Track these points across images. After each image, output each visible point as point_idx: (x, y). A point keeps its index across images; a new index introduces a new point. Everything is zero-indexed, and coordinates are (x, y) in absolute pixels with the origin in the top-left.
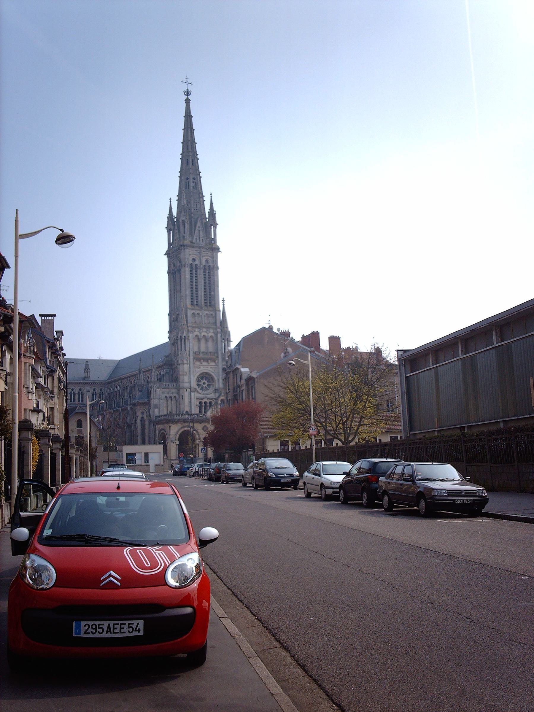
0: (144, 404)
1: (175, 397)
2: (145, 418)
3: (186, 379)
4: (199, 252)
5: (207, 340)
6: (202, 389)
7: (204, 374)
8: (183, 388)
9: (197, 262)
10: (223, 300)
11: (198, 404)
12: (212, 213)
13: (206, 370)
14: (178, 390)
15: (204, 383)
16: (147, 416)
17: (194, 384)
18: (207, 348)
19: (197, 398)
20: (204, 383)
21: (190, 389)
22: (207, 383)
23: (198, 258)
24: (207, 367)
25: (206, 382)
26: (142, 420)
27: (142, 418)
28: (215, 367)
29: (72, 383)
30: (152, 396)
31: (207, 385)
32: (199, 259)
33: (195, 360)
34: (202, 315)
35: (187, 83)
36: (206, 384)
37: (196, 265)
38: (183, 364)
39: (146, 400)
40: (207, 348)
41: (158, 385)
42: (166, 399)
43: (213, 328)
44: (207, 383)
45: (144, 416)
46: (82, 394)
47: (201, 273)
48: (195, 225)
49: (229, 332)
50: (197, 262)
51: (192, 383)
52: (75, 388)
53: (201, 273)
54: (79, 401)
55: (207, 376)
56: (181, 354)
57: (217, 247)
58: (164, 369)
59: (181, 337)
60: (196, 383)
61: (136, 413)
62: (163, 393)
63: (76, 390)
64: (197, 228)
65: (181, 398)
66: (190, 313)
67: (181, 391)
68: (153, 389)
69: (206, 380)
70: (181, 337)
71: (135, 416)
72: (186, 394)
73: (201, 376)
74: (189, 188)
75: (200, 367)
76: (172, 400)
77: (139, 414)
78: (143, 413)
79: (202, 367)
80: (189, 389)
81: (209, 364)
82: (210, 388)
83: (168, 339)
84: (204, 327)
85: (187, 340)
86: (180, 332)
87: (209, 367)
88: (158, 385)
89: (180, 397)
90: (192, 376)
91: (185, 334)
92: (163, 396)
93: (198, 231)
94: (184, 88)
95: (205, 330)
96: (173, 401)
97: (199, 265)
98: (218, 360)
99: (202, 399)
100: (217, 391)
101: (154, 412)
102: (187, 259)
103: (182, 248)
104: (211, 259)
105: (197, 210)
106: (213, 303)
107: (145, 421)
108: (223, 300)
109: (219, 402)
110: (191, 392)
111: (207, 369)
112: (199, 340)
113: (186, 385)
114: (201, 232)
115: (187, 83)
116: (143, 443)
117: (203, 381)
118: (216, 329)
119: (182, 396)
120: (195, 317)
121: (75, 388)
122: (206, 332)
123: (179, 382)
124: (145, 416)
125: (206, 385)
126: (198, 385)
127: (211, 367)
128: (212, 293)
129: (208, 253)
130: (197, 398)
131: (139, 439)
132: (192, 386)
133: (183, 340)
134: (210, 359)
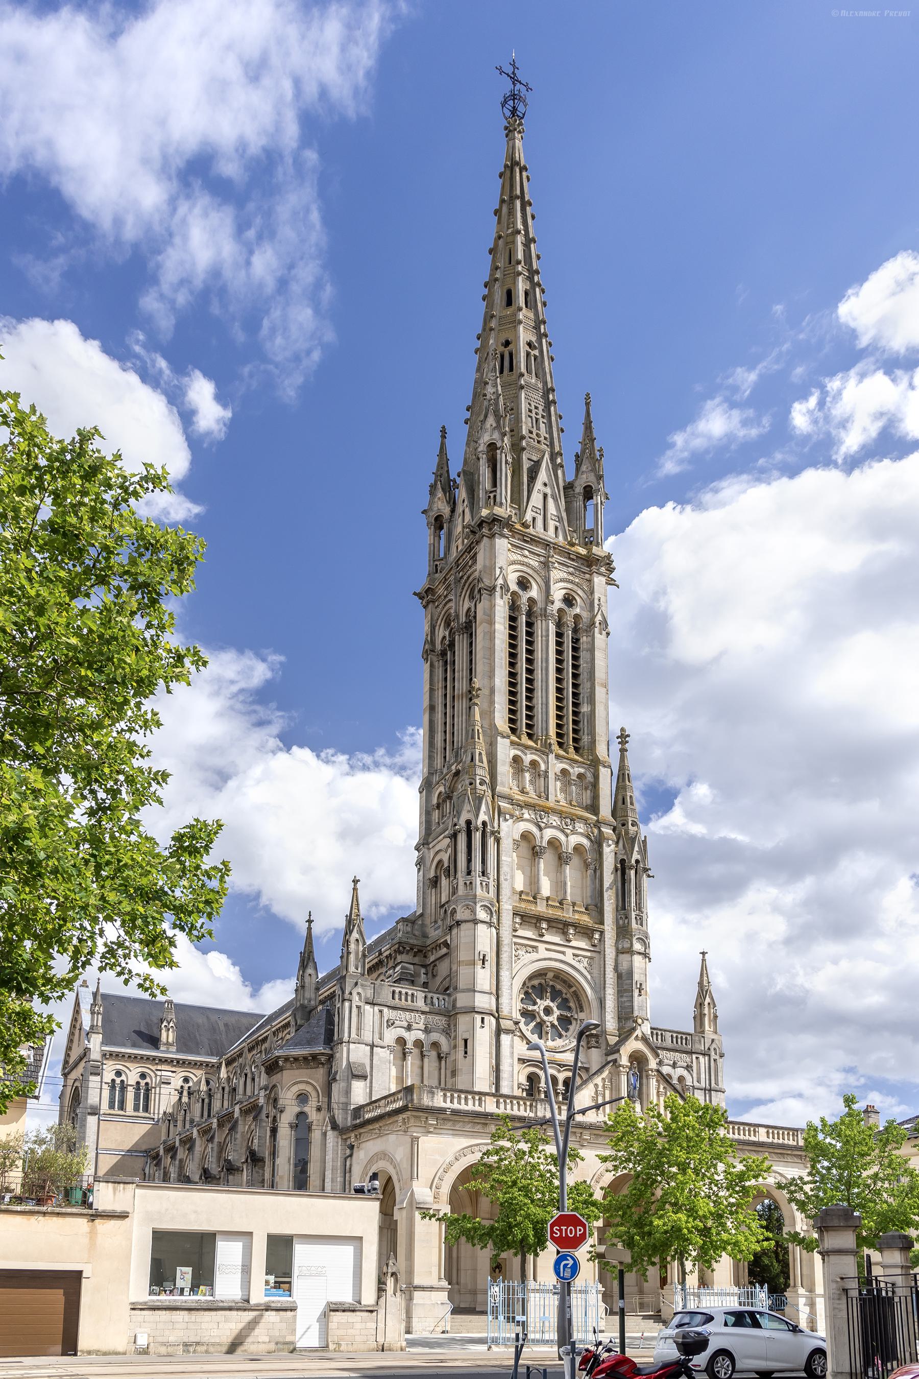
0: (312, 1060)
1: (435, 1045)
2: (313, 1116)
3: (484, 978)
4: (542, 559)
5: (562, 859)
6: (540, 1029)
7: (550, 975)
8: (472, 1010)
9: (534, 592)
11: (523, 1080)
13: (556, 960)
14: (451, 1014)
15: (548, 1011)
16: (319, 1109)
17: (512, 1004)
19: (519, 1059)
20: (548, 1011)
21: (497, 1019)
22: (557, 1013)
23: (539, 579)
24: (563, 953)
25: (553, 1005)
26: (301, 1124)
27: (301, 1115)
28: (590, 958)
29: (123, 1056)
30: (348, 1027)
31: (558, 1019)
32: (543, 584)
33: (518, 920)
34: (546, 772)
35: (514, 80)
36: (555, 1016)
37: (531, 601)
38: (475, 922)
39: (320, 1049)
41: (369, 993)
42: (398, 1048)
43: (585, 821)
44: (557, 1013)
45: (306, 1109)
46: (148, 1090)
47: (547, 632)
48: (532, 478)
50: (534, 592)
51: (504, 1000)
52: (127, 1071)
53: (547, 632)
54: (136, 1108)
55: (558, 987)
56: (470, 885)
58: (394, 968)
59: (468, 823)
60: (520, 1006)
61: (275, 1100)
62: (391, 1024)
63: (132, 1076)
64: (538, 485)
65: (461, 1048)
66: (505, 751)
67: (462, 1020)
68: (347, 1004)
69: (552, 1001)
70: (468, 823)
71: (273, 1112)
72: (483, 1037)
73: (536, 982)
76: (422, 1056)
77: (288, 1097)
78: (302, 1098)
79: (542, 947)
80: (493, 1021)
81: (569, 941)
82: (567, 1030)
84: (554, 811)
85: (491, 841)
86: (466, 807)
87: (569, 952)
88: (369, 993)
89: (455, 1047)
90: (505, 974)
91: (483, 817)
92: (390, 1036)
93: (541, 497)
94: (507, 86)
95: (555, 820)
96: (426, 1060)
97: (540, 605)
99: (540, 1064)
100: (593, 1042)
101: (348, 1092)
102: (501, 568)
103: (485, 531)
105: (538, 435)
106: (585, 739)
107: (309, 1128)
109: (624, 1061)
110: (499, 1031)
111: (560, 957)
112: (535, 853)
113: (483, 1001)
114: (551, 503)
115: (514, 80)
116: (301, 1183)
117: (542, 1004)
118: (598, 824)
119: (466, 1041)
120: (522, 770)
121: (127, 1071)
123: (456, 988)
124: (310, 1109)
125: (553, 1018)
126: (525, 1013)
127: (574, 955)
130: (522, 1061)
131: (284, 1164)
132: (505, 1011)
133: (477, 836)
134: (575, 926)
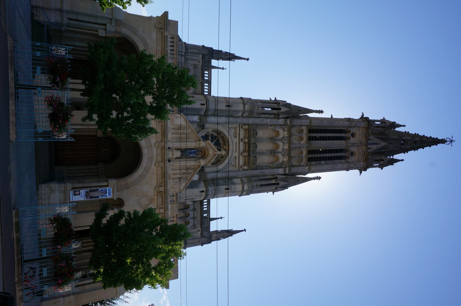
10: (319, 178)
12: (393, 162)
18: (262, 153)
24: (236, 152)
33: (246, 127)
40: (262, 153)
47: (84, 245)
49: (284, 190)
57: (390, 123)
74: (155, 24)
75: (236, 137)
83: (433, 137)
87: (237, 155)
95: (286, 147)
98: (248, 170)
104: (356, 160)
108: (319, 178)
122: (283, 149)
127: (236, 158)
128: (323, 162)
129: (361, 154)
